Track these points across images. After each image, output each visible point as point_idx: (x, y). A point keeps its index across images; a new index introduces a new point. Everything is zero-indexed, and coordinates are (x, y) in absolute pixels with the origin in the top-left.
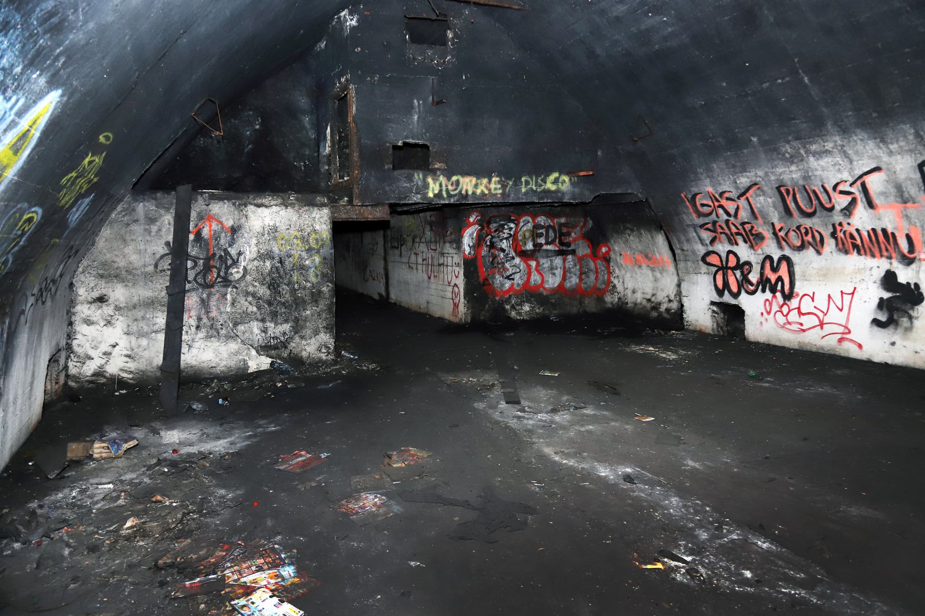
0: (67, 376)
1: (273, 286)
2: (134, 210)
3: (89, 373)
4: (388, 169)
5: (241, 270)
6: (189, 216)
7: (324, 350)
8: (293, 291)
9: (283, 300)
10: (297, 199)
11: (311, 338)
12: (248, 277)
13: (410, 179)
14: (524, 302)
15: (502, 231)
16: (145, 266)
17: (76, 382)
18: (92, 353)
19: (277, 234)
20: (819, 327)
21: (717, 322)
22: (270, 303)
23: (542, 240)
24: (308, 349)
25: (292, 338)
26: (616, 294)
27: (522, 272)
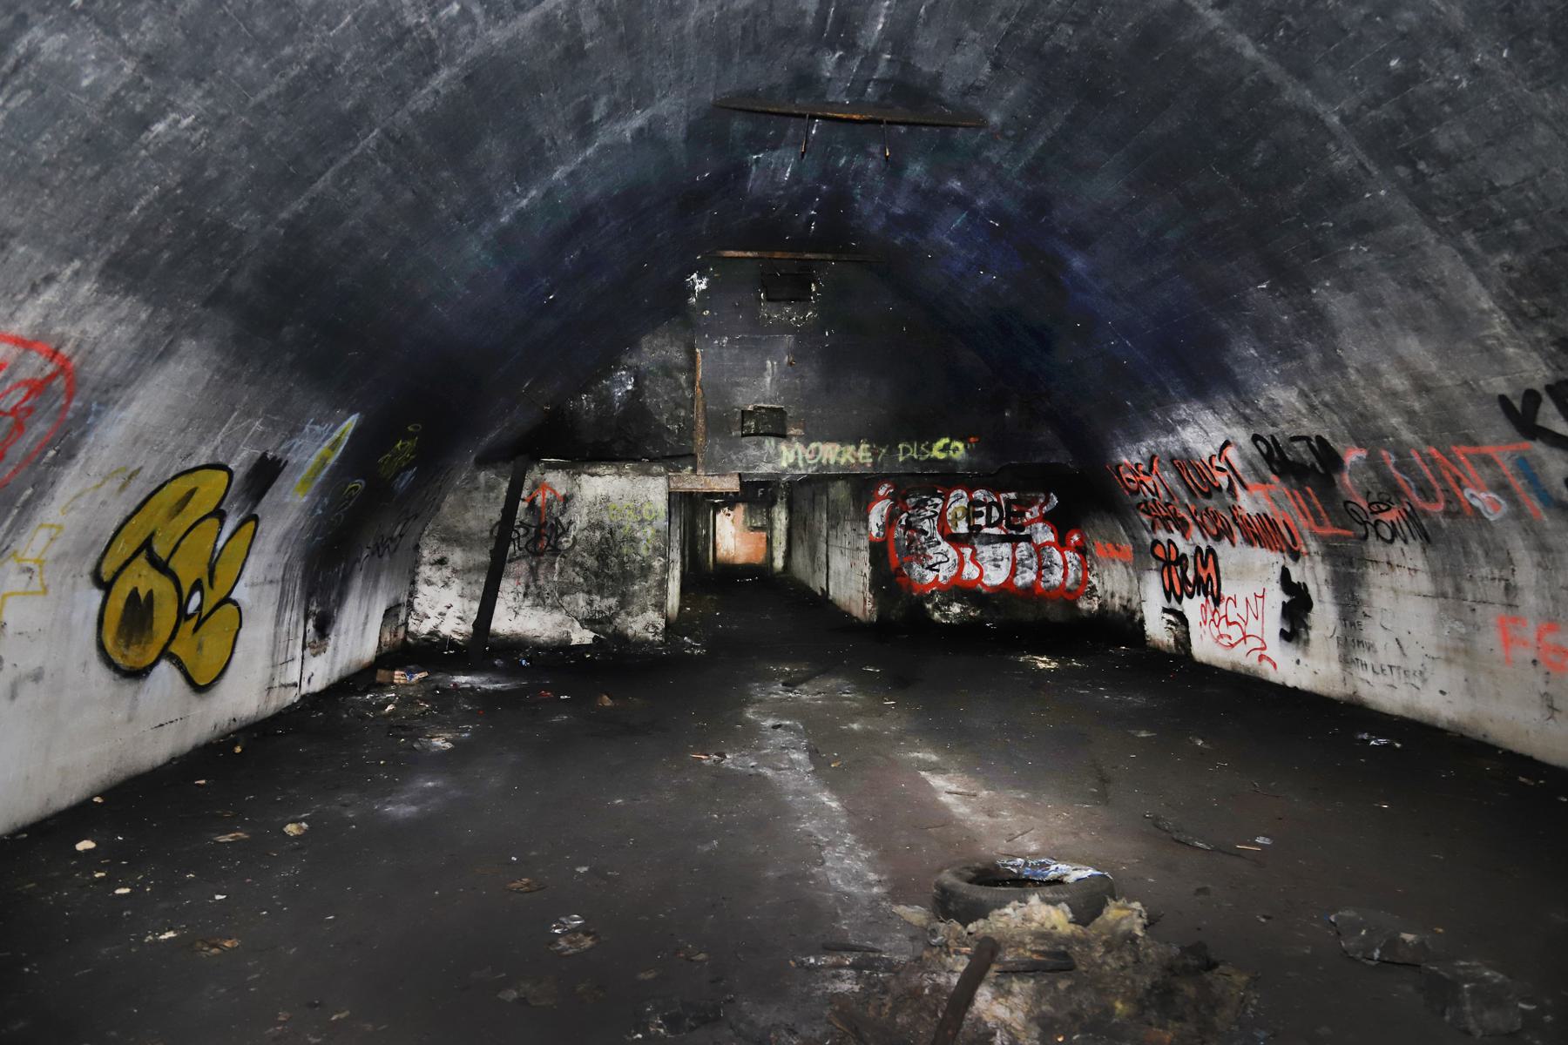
0: (407, 632)
1: (602, 557)
2: (476, 478)
3: (425, 632)
4: (736, 436)
5: (570, 539)
6: (522, 486)
7: (651, 630)
8: (622, 564)
9: (610, 573)
10: (632, 469)
11: (637, 615)
12: (577, 547)
13: (759, 446)
14: (952, 601)
15: (923, 508)
16: (482, 532)
17: (414, 639)
18: (430, 612)
19: (609, 504)
20: (1243, 641)
21: (1175, 636)
22: (597, 575)
23: (981, 521)
24: (635, 627)
25: (617, 614)
26: (1096, 599)
27: (951, 561)
